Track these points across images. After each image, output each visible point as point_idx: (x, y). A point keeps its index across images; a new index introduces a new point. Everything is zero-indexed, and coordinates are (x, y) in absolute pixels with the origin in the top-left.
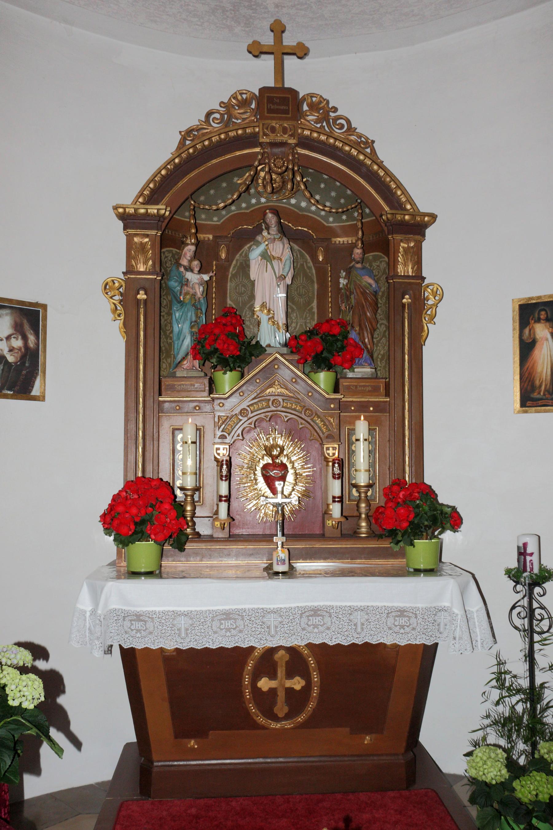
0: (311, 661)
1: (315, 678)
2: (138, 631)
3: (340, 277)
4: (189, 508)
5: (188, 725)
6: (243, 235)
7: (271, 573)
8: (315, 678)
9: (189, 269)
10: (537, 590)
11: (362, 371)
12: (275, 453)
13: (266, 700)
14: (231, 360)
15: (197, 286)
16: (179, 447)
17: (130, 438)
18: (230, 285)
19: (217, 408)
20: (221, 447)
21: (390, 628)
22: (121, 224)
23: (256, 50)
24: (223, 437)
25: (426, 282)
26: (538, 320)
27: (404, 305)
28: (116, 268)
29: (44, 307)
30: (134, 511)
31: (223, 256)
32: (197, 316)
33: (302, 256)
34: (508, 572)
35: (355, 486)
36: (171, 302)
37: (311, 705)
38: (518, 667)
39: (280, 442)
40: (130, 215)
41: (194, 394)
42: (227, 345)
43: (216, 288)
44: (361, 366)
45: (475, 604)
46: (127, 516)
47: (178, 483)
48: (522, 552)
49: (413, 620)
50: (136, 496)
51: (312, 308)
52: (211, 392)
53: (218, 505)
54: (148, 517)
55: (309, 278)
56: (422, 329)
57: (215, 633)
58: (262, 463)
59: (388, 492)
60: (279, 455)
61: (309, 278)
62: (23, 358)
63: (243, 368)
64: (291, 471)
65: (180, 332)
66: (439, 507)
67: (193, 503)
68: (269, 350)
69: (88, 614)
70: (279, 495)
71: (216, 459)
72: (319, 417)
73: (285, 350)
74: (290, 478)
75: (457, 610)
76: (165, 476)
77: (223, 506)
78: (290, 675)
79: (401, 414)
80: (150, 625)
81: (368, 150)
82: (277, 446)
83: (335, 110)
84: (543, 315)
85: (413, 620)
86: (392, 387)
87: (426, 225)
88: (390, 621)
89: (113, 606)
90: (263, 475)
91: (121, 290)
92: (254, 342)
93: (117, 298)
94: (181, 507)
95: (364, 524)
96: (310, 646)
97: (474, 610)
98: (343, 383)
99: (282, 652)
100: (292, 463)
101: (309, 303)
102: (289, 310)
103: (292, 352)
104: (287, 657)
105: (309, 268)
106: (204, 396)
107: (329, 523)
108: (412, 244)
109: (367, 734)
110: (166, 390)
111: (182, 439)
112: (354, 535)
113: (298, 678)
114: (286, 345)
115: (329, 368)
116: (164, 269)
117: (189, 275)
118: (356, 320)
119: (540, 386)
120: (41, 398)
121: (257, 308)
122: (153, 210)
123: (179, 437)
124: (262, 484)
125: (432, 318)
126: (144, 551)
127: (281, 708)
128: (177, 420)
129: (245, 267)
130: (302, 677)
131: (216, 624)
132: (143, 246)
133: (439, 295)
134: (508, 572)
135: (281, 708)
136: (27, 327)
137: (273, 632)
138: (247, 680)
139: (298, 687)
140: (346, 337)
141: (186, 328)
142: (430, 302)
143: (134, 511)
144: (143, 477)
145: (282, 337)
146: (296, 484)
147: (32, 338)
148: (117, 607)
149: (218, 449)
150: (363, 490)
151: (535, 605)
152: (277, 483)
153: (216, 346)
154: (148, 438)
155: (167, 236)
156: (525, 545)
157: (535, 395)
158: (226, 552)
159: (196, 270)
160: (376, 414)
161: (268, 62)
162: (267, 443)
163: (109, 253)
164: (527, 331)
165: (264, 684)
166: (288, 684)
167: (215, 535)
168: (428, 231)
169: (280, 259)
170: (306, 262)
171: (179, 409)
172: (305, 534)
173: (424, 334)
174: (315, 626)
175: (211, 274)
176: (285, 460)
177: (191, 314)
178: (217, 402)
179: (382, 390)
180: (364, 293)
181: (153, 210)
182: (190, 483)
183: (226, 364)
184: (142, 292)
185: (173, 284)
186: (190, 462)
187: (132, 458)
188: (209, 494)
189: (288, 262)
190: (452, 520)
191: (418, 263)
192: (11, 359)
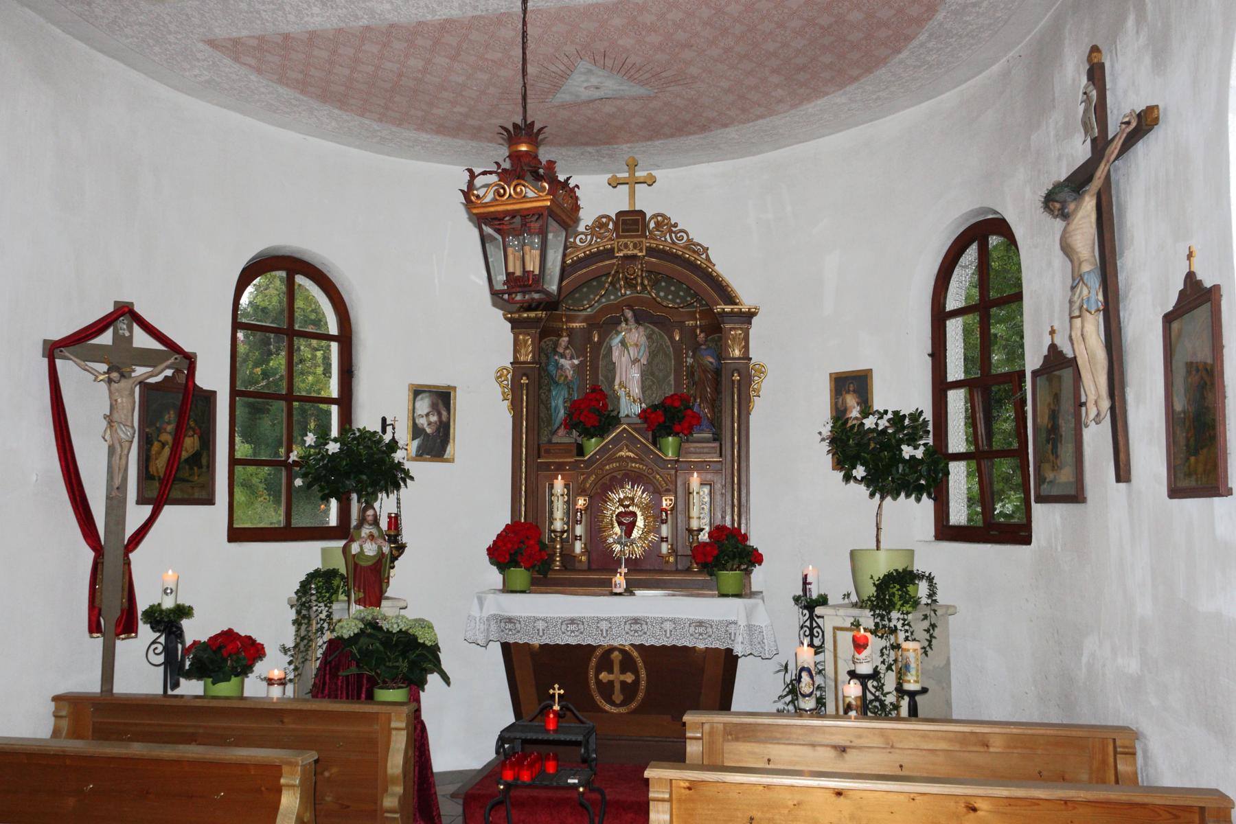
0: (640, 663)
1: (643, 674)
6: (608, 323)
8: (643, 674)
9: (563, 356)
13: (606, 690)
14: (592, 430)
22: (509, 325)
23: (615, 183)
26: (848, 392)
27: (733, 381)
28: (507, 359)
29: (454, 388)
33: (662, 337)
37: (641, 695)
44: (702, 431)
48: (805, 582)
49: (709, 630)
54: (523, 552)
55: (666, 355)
61: (666, 355)
62: (438, 430)
78: (623, 672)
80: (518, 625)
83: (675, 225)
85: (709, 630)
88: (692, 629)
96: (640, 648)
99: (616, 653)
101: (667, 376)
114: (639, 415)
116: (544, 355)
117: (562, 361)
120: (451, 460)
126: (520, 575)
127: (618, 697)
131: (564, 627)
133: (762, 371)
135: (618, 697)
136: (441, 406)
138: (592, 673)
141: (560, 401)
145: (637, 409)
147: (444, 413)
161: (624, 189)
165: (604, 676)
166: (622, 677)
168: (754, 320)
174: (636, 631)
191: (746, 347)
192: (429, 431)
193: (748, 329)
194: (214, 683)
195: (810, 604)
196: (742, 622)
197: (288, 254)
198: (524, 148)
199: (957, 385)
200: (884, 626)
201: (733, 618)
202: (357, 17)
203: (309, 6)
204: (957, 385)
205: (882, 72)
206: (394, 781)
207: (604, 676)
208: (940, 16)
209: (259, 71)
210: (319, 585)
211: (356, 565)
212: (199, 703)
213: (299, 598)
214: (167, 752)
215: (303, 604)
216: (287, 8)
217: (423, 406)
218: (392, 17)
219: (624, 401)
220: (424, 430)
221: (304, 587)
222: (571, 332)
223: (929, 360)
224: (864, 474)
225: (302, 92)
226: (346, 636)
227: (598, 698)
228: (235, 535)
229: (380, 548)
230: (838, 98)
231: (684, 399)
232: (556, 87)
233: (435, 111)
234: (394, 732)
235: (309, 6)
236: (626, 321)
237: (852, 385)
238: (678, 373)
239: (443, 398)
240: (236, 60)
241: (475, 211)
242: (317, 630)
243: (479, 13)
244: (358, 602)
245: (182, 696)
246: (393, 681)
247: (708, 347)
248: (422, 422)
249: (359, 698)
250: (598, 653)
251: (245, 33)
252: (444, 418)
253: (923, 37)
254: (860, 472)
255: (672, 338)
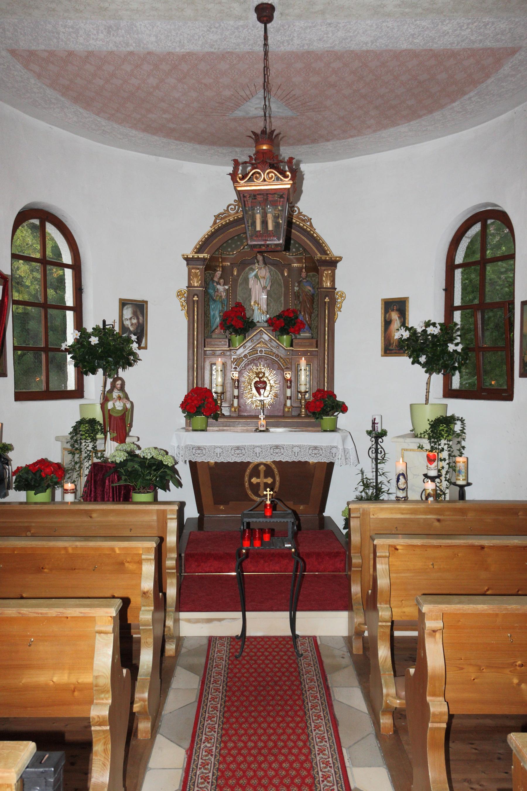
0: (276, 471)
1: (278, 478)
2: (199, 454)
3: (295, 286)
4: (219, 402)
5: (220, 499)
6: (244, 264)
7: (257, 430)
8: (278, 478)
9: (218, 283)
10: (380, 440)
11: (305, 334)
12: (261, 376)
13: (255, 488)
14: (239, 330)
15: (222, 293)
16: (214, 372)
17: (190, 369)
18: (239, 289)
19: (232, 354)
20: (235, 373)
21: (310, 455)
22: (185, 262)
24: (235, 368)
25: (337, 290)
26: (393, 310)
27: (325, 302)
28: (183, 285)
30: (196, 402)
31: (235, 273)
32: (222, 306)
34: (367, 431)
35: (300, 392)
36: (209, 299)
38: (370, 475)
39: (263, 371)
40: (190, 258)
41: (221, 346)
42: (238, 323)
43: (232, 292)
44: (305, 332)
45: (349, 445)
46: (193, 404)
47: (213, 390)
48: (374, 423)
49: (321, 451)
50: (196, 396)
51: (281, 301)
52: (229, 346)
53: (233, 401)
54: (200, 405)
56: (335, 314)
57: (233, 455)
58: (254, 381)
59: (314, 395)
60: (263, 377)
62: (137, 328)
63: (245, 334)
64: (268, 385)
65: (214, 315)
66: (336, 402)
67: (221, 400)
68: (258, 324)
69: (176, 448)
70: (262, 396)
71: (232, 379)
72: (282, 358)
73: (266, 325)
74: (268, 388)
75: (340, 447)
76: (207, 386)
77: (236, 401)
78: (266, 477)
79: (323, 357)
81: (308, 223)
82: (261, 372)
84: (395, 308)
85: (321, 451)
86: (319, 343)
87: (337, 262)
88: (310, 451)
89: (188, 443)
90: (255, 387)
91: (185, 295)
92: (250, 320)
93: (183, 299)
94: (216, 401)
95: (303, 410)
96: (274, 462)
97: (350, 448)
98: (295, 341)
99: (262, 466)
100: (269, 380)
102: (269, 302)
103: (270, 326)
104: (265, 468)
105: (280, 279)
106: (226, 348)
107: (286, 409)
108: (330, 272)
109: (302, 504)
110: (207, 345)
111: (216, 369)
112: (299, 416)
113: (270, 478)
114: (267, 321)
115: (287, 334)
116: (207, 282)
117: (219, 287)
118: (302, 310)
119: (393, 343)
121: (252, 303)
122: (201, 256)
123: (214, 367)
124: (254, 391)
125: (340, 309)
126: (200, 419)
128: (213, 360)
129: (246, 280)
130: (272, 478)
131: (233, 451)
132: (196, 274)
134: (367, 431)
136: (139, 313)
137: (258, 456)
138: (246, 479)
139: (269, 482)
140: (297, 318)
141: (217, 313)
142: (339, 301)
143: (196, 402)
144: (197, 387)
145: (264, 318)
146: (271, 391)
147: (141, 318)
148: (190, 444)
149: (233, 374)
150: (303, 394)
151: (379, 447)
152: (261, 390)
153: (232, 323)
154: (199, 368)
155: (209, 267)
156: (375, 419)
157: (391, 348)
158: (237, 423)
159: (222, 284)
160: (310, 357)
162: (257, 371)
163: (179, 278)
164: (387, 315)
165: (254, 480)
167: (232, 415)
168: (339, 265)
169: (264, 278)
170: (278, 276)
171: (214, 354)
172: (277, 417)
173: (336, 317)
174: (277, 453)
175: (229, 285)
176: (265, 379)
177: (219, 306)
178: (232, 351)
179: (315, 345)
180: (306, 295)
181: (201, 256)
182: (220, 390)
183: (237, 332)
184: (195, 297)
185: (211, 291)
186: (220, 380)
187: (191, 378)
188: (228, 395)
189: (268, 280)
190: (343, 408)
191: (333, 281)
193: (334, 270)
194: (35, 494)
195: (377, 435)
196: (340, 447)
197: (42, 208)
198: (265, 147)
199: (458, 308)
200: (436, 448)
201: (335, 444)
202: (127, 44)
203: (98, 33)
204: (458, 308)
205: (437, 115)
206: (171, 550)
207: (254, 480)
208: (489, 81)
209: (39, 76)
210: (86, 428)
211: (110, 416)
212: (22, 507)
213: (72, 438)
214: (92, 544)
215: (76, 441)
216: (81, 32)
217: (128, 313)
218: (152, 48)
219: (257, 312)
220: (129, 328)
221: (76, 429)
222: (223, 268)
223: (443, 293)
224: (93, 343)
225: (63, 95)
226: (118, 462)
227: (249, 492)
228: (19, 396)
229: (125, 404)
230: (403, 128)
231: (294, 311)
232: (238, 106)
233: (150, 116)
234: (169, 521)
235: (98, 33)
236: (258, 262)
237: (396, 307)
238: (286, 295)
239: (140, 308)
240: (26, 67)
241: (239, 189)
242: (85, 458)
243: (213, 50)
244: (113, 439)
245: (9, 503)
246: (144, 489)
247: (307, 281)
248: (127, 323)
249: (120, 501)
250: (251, 466)
251: (42, 47)
252: (141, 321)
253: (472, 94)
254: (423, 359)
255: (283, 274)
